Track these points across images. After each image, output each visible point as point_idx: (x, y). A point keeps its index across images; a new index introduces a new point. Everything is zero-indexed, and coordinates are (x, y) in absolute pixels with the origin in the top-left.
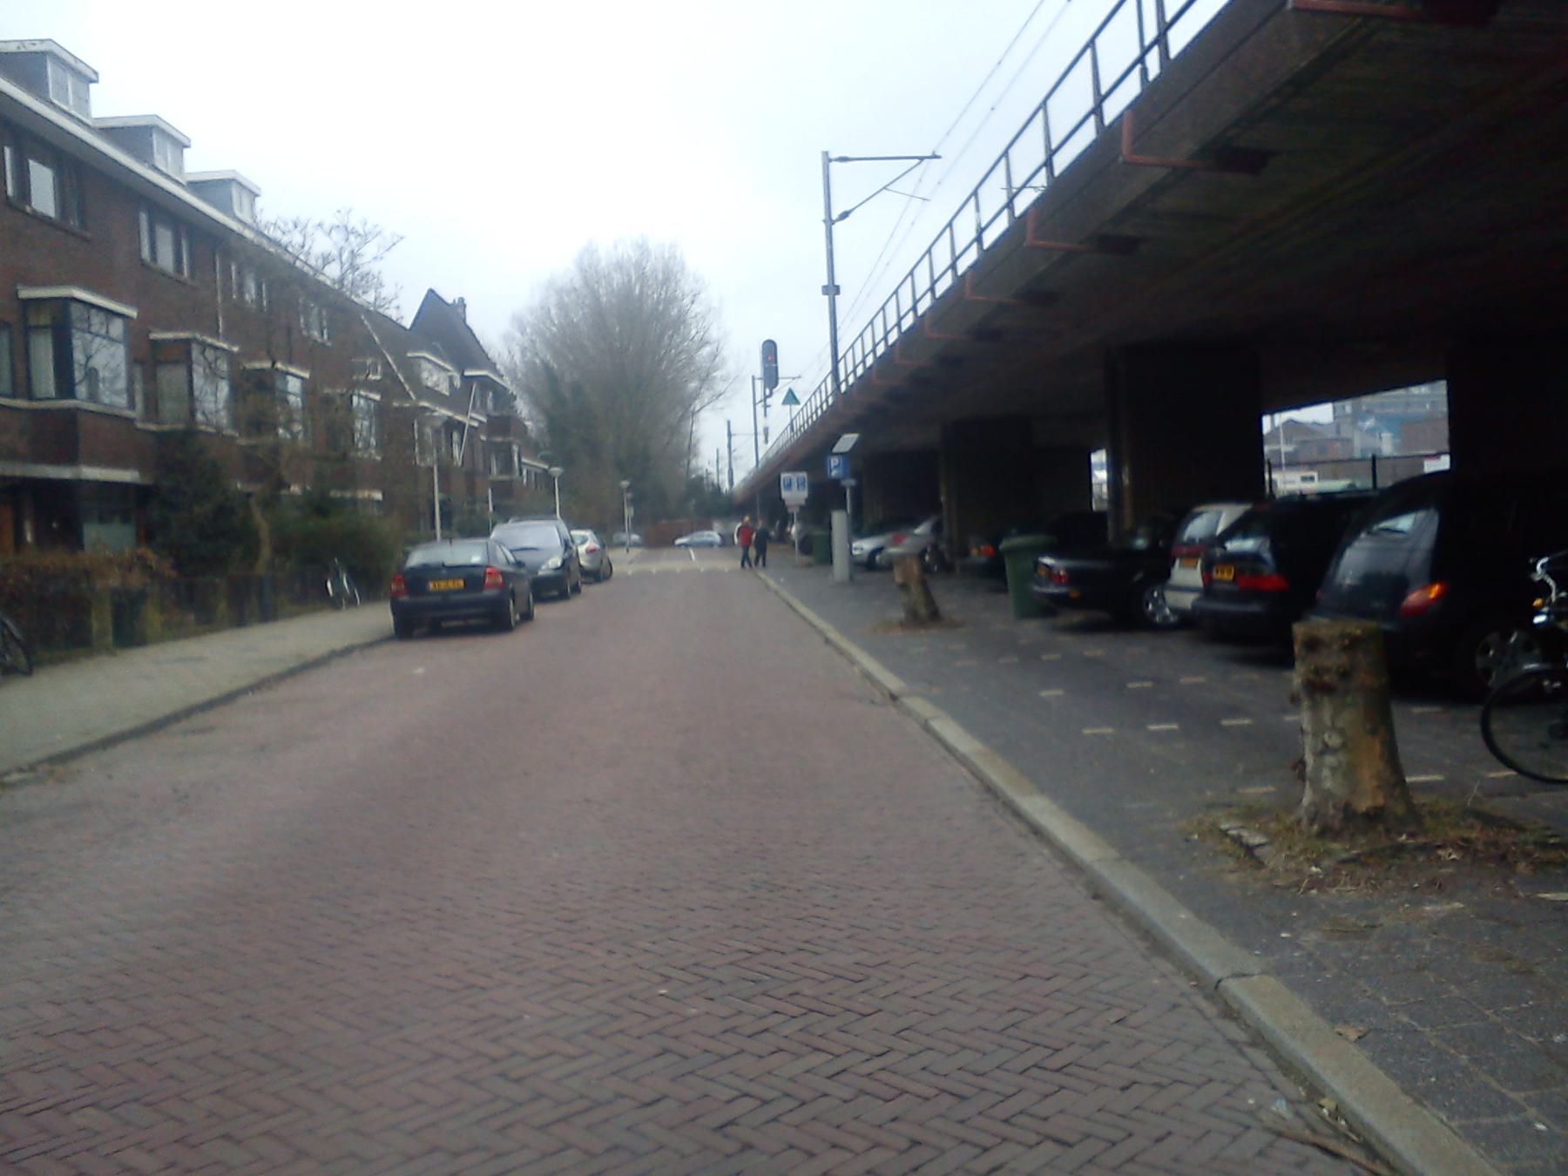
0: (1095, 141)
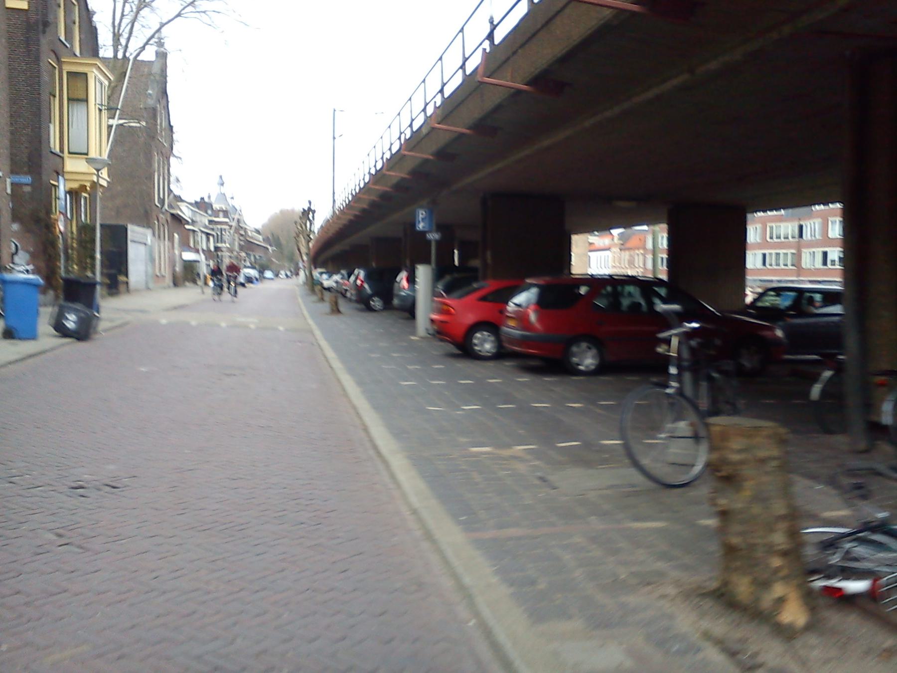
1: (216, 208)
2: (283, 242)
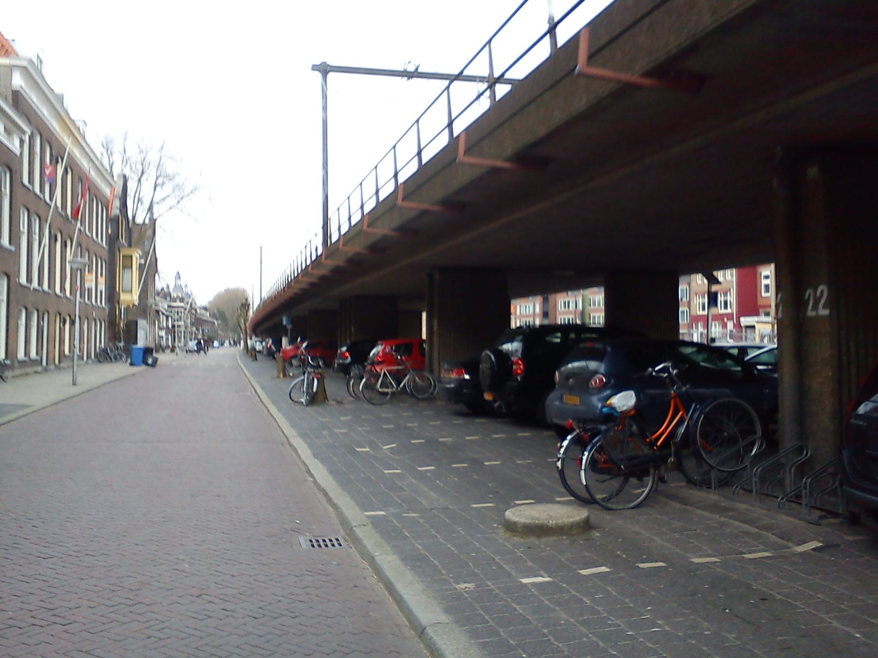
0: (489, 110)
1: (174, 297)
2: (228, 315)
